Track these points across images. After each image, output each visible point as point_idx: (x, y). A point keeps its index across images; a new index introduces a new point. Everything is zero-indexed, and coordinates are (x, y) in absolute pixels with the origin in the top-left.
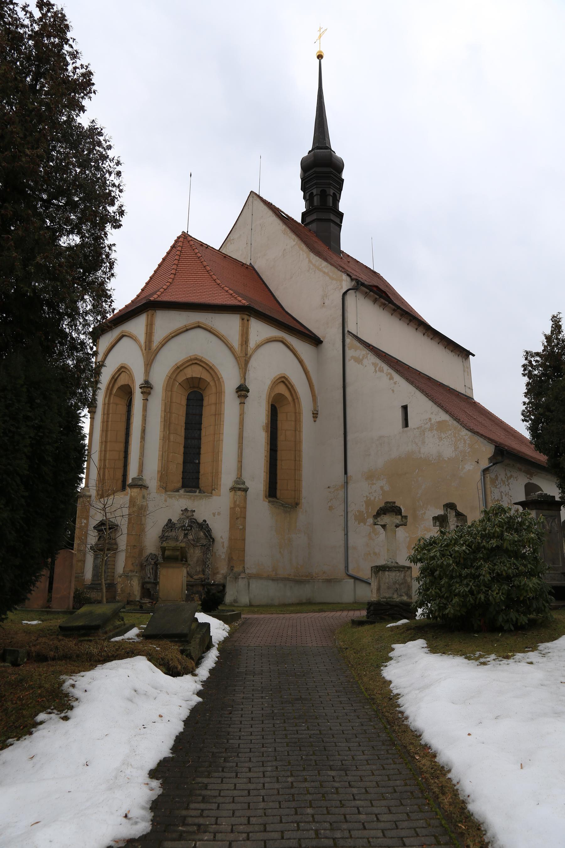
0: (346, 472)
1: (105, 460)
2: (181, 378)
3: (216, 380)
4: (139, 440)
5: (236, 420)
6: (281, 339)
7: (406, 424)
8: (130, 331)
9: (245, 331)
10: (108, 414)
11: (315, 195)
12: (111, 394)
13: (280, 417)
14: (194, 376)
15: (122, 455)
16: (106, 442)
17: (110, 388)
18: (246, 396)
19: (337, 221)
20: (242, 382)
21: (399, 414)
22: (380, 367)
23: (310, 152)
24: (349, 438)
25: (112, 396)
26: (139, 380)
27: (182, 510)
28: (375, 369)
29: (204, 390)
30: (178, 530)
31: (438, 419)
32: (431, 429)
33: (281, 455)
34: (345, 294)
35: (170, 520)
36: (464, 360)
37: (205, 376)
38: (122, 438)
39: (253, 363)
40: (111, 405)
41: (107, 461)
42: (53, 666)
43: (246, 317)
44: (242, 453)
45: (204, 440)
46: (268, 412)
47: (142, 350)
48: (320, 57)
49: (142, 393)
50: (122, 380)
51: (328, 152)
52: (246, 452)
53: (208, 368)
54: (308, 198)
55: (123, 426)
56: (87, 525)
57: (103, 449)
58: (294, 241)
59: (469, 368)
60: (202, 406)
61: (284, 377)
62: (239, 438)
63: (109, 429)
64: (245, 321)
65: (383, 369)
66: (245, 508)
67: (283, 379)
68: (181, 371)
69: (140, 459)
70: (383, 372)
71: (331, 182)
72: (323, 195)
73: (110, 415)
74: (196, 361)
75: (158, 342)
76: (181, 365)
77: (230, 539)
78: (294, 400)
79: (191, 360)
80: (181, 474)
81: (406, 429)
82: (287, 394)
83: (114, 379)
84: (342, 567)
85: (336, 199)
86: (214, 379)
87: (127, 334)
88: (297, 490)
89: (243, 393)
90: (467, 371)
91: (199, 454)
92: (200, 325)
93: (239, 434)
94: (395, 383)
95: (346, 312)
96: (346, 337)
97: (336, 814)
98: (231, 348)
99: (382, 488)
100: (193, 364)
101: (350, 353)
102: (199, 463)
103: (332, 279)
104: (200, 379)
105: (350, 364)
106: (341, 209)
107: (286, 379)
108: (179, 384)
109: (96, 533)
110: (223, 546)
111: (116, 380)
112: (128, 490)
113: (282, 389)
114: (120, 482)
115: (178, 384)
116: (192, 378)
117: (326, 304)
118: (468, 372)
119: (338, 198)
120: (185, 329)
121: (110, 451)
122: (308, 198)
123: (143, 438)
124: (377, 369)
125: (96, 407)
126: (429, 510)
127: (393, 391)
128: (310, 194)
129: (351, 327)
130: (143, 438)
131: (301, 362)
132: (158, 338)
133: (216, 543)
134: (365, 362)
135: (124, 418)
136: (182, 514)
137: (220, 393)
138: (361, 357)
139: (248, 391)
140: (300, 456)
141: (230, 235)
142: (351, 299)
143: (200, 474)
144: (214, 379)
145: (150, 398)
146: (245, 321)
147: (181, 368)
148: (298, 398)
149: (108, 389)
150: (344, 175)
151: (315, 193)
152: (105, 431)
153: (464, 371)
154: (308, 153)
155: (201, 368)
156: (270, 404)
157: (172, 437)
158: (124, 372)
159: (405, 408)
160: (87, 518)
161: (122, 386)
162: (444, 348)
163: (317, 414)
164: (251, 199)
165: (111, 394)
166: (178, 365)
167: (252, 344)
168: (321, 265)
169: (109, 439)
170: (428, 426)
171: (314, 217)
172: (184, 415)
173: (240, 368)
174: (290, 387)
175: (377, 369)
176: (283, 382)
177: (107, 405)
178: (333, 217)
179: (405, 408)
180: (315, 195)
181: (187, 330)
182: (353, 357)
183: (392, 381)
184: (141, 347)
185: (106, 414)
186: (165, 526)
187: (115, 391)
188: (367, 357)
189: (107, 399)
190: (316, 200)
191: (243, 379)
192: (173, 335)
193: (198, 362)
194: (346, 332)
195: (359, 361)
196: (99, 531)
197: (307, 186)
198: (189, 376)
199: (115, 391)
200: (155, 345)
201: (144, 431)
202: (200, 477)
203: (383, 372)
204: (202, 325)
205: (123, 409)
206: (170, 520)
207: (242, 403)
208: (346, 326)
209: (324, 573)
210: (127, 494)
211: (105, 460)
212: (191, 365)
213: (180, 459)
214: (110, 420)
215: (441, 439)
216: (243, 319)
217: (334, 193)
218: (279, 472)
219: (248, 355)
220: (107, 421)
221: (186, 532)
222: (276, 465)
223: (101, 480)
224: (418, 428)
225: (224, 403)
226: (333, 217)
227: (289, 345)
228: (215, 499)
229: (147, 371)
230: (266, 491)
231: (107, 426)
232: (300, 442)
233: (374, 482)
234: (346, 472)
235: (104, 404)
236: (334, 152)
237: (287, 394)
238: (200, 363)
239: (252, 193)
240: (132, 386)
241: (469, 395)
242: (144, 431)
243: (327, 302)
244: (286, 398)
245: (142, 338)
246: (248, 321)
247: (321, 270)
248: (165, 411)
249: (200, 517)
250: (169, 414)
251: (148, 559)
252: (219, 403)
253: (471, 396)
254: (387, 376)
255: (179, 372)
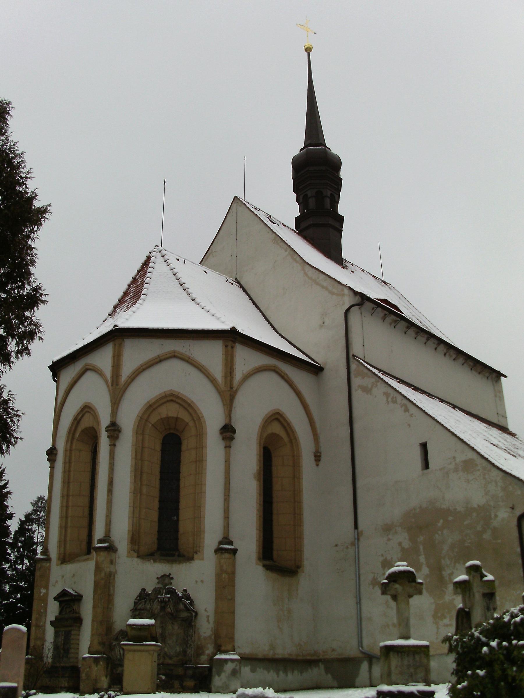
0: (356, 527)
1: (67, 517)
2: (154, 418)
3: (195, 419)
4: (105, 493)
5: (221, 468)
6: (273, 368)
7: (426, 465)
8: (95, 363)
9: (229, 360)
10: (70, 462)
11: (310, 197)
12: (73, 438)
13: (276, 462)
14: (171, 415)
15: (87, 511)
16: (68, 496)
17: (72, 432)
18: (232, 439)
19: (337, 225)
20: (227, 422)
21: (417, 452)
22: (393, 398)
23: (302, 150)
24: (359, 484)
25: (75, 441)
26: (105, 421)
27: (157, 578)
28: (387, 400)
29: (182, 432)
30: (153, 602)
31: (464, 458)
32: (456, 470)
33: (277, 507)
34: (347, 311)
35: (143, 590)
36: (494, 382)
37: (184, 415)
38: (86, 491)
39: (240, 399)
40: (73, 453)
41: (69, 519)
42: (46, 650)
43: (230, 344)
44: (228, 507)
45: (183, 492)
46: (260, 456)
47: (108, 386)
48: (308, 50)
49: (108, 437)
50: (87, 422)
51: (322, 149)
52: (234, 504)
53: (186, 406)
54: (302, 200)
55: (87, 476)
56: (47, 594)
57: (65, 504)
58: (286, 251)
59: (501, 392)
60: (180, 451)
61: (278, 413)
62: (225, 489)
63: (72, 480)
64: (229, 348)
65: (396, 399)
66: (234, 573)
67: (277, 416)
68: (154, 409)
69: (107, 516)
70: (397, 403)
71: (327, 182)
72: (319, 197)
73: (73, 464)
74: (171, 398)
75: (126, 377)
76: (155, 403)
77: (216, 613)
78: (291, 441)
79: (166, 396)
80: (156, 533)
81: (426, 471)
82: (282, 433)
83: (77, 421)
84: (354, 642)
85: (335, 200)
86: (193, 419)
87: (91, 367)
88: (298, 549)
89: (229, 434)
90: (499, 394)
91: (177, 509)
92: (176, 354)
93: (225, 484)
94: (411, 415)
95: (349, 332)
96: (351, 363)
97: (405, 303)
98: (213, 381)
99: (400, 544)
100: (168, 401)
101: (356, 381)
102: (178, 520)
103: (332, 293)
104: (177, 419)
105: (357, 394)
106: (340, 212)
107: (281, 416)
108: (153, 425)
109: (57, 604)
110: (208, 621)
111: (78, 422)
112: (94, 553)
113: (276, 428)
114: (84, 546)
115: (151, 425)
116: (168, 418)
117: (326, 324)
118: (500, 397)
119: (337, 200)
120: (158, 360)
121: (72, 506)
122: (301, 200)
123: (110, 491)
124: (390, 399)
125: (56, 454)
126: (457, 569)
127: (409, 425)
128: (303, 197)
129: (356, 349)
130: (110, 491)
131: (298, 394)
132: (127, 370)
133: (199, 617)
134: (375, 391)
135: (89, 467)
136: (158, 583)
137: (201, 435)
138: (370, 386)
139: (234, 431)
140: (300, 508)
141: (212, 246)
142: (355, 317)
143: (180, 533)
144: (193, 419)
145: (118, 444)
146: (229, 348)
147: (154, 407)
148: (295, 438)
149: (69, 432)
150: (343, 174)
151: (309, 195)
152: (67, 482)
153: (496, 396)
154: (300, 151)
155: (176, 406)
156: (262, 446)
157: (144, 490)
158: (89, 412)
159: (424, 446)
160: (47, 587)
161: (86, 429)
162: (469, 369)
163: (320, 456)
164: (235, 205)
165: (73, 438)
166: (151, 403)
167: (238, 376)
168: (318, 278)
169: (71, 493)
170: (452, 466)
171: (310, 222)
172: (159, 462)
173: (224, 405)
174: (286, 425)
175: (390, 399)
176: (277, 419)
177: (69, 451)
178: (331, 222)
179: (424, 446)
180: (310, 197)
181: (159, 360)
182: (360, 387)
183: (407, 413)
184: (106, 382)
185: (68, 462)
186: (137, 597)
187: (77, 435)
188: (377, 386)
189: (69, 444)
190: (312, 203)
191: (228, 417)
192: (144, 367)
193: (174, 399)
194: (351, 356)
195: (367, 390)
196: (61, 602)
197: (300, 187)
198: (164, 416)
199: (77, 435)
200: (124, 378)
201: (111, 483)
202: (179, 537)
203: (397, 403)
204: (178, 355)
205: (86, 456)
206: (143, 590)
207: (228, 447)
208: (350, 349)
209: (333, 650)
210: (92, 559)
211: (67, 517)
212: (165, 402)
213: (155, 515)
214: (72, 469)
215: (468, 481)
216: (226, 346)
217: (331, 194)
218: (275, 528)
219: (235, 389)
220: (69, 471)
221: (163, 604)
222: (271, 521)
223: (63, 541)
224: (440, 470)
225: (206, 447)
226: (331, 222)
227: (283, 374)
228: (196, 564)
229: (114, 412)
230: (259, 553)
231: (69, 476)
232: (300, 491)
233: (390, 536)
234: (356, 527)
235: (66, 451)
236: (330, 149)
237: (282, 433)
238: (177, 400)
239: (236, 199)
240: (97, 429)
241: (502, 425)
242: (111, 483)
243: (327, 321)
244: (282, 438)
245: (108, 373)
246: (232, 347)
247: (318, 284)
248: (136, 459)
249: (179, 588)
250: (140, 461)
251: (117, 637)
252: (201, 447)
253: (505, 426)
254: (401, 407)
255: (152, 412)
